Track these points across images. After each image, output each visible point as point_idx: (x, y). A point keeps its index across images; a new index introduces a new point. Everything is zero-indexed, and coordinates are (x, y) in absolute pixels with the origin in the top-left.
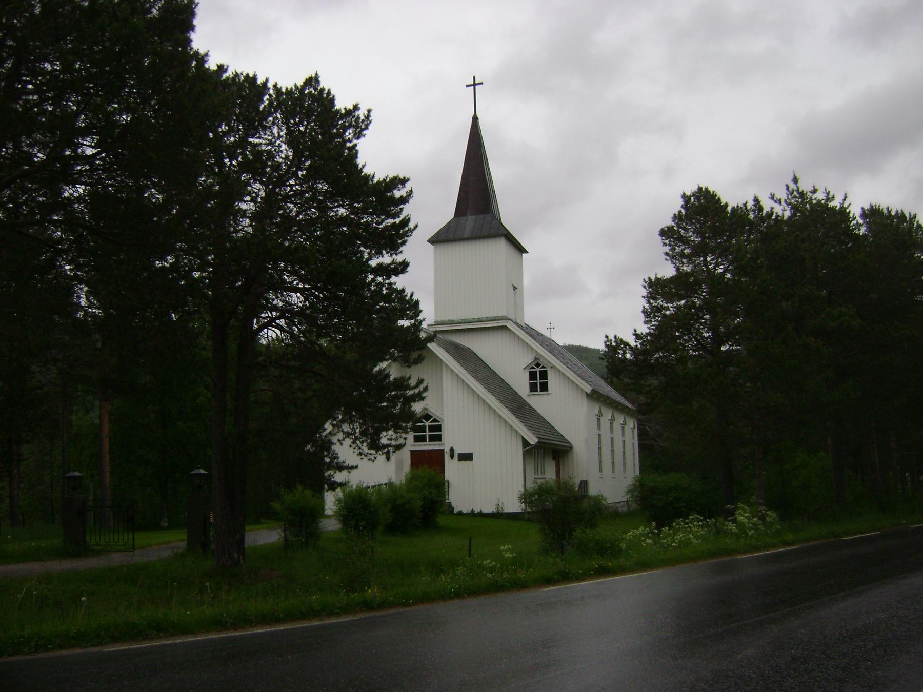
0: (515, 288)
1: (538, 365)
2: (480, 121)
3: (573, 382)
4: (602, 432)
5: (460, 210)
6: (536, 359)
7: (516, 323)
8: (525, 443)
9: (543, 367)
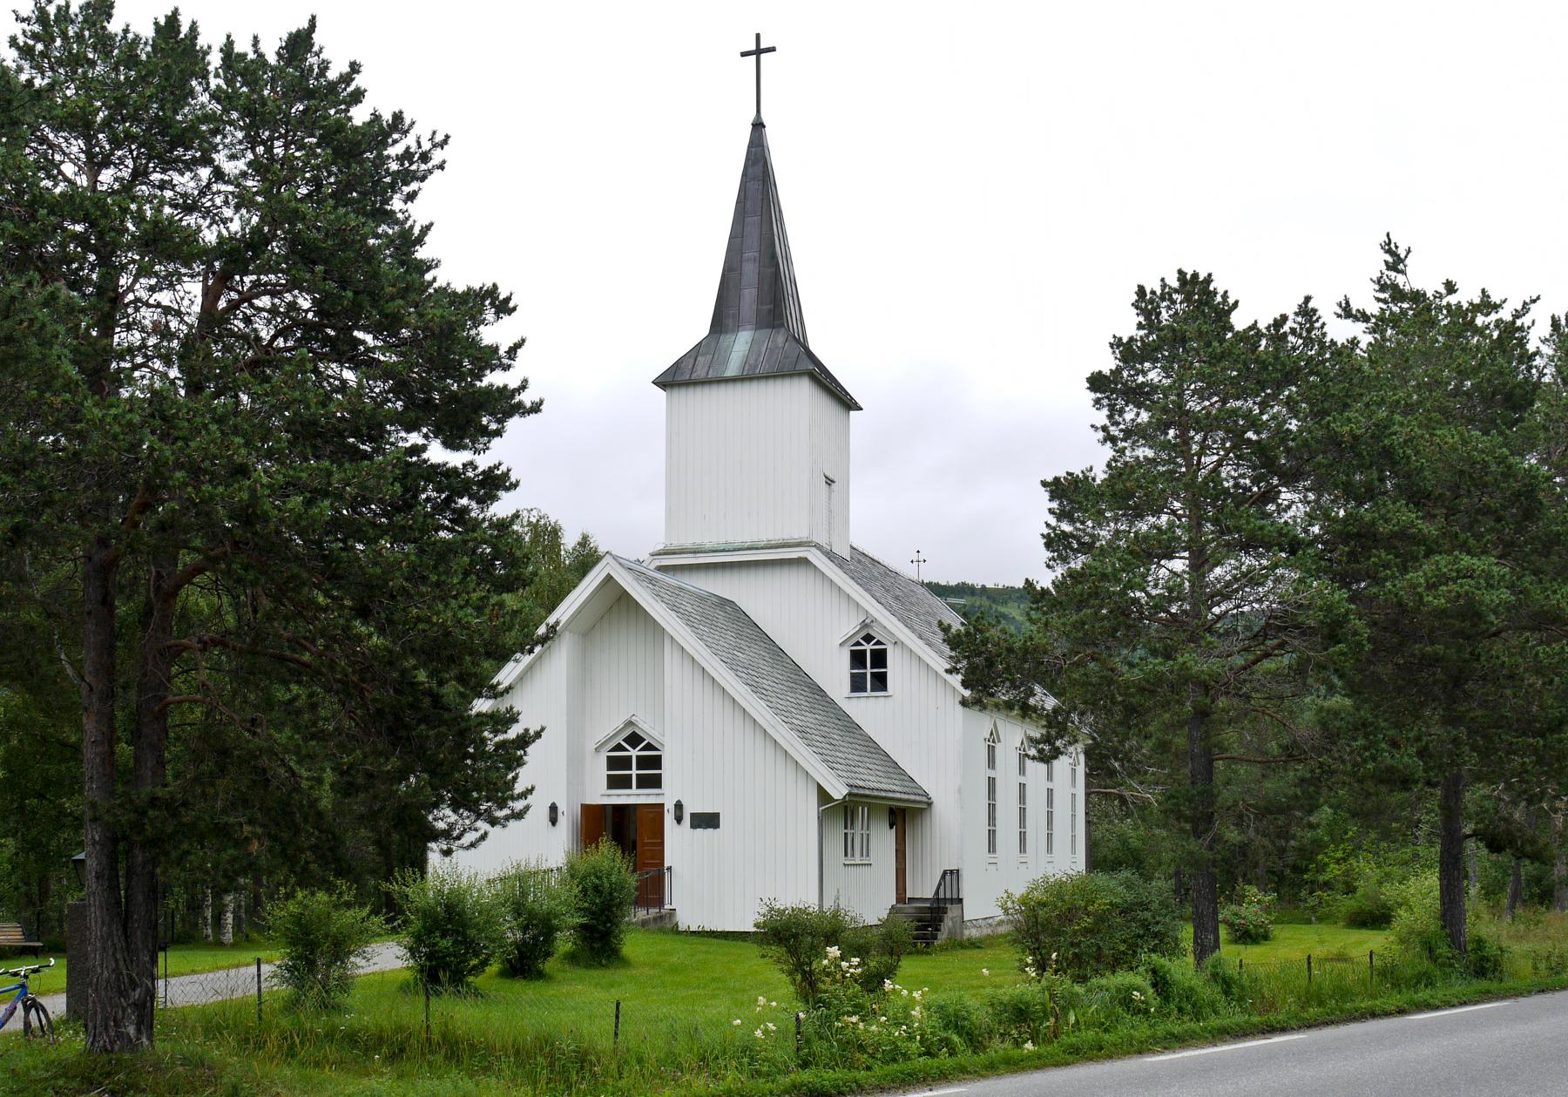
0: (830, 482)
1: (868, 638)
2: (771, 134)
4: (1055, 785)
5: (722, 321)
6: (864, 625)
7: (830, 555)
8: (823, 796)
9: (879, 643)
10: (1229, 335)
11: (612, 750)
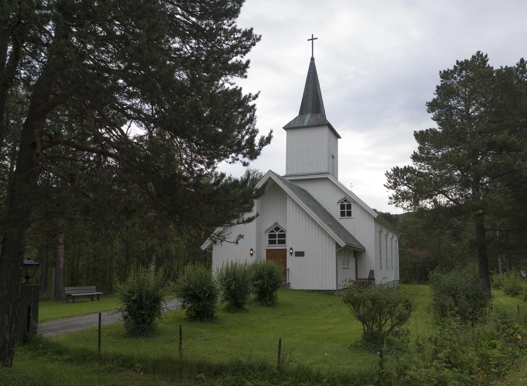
0: (333, 157)
1: (346, 201)
3: (326, 232)
5: (303, 111)
8: (338, 246)
9: (349, 202)
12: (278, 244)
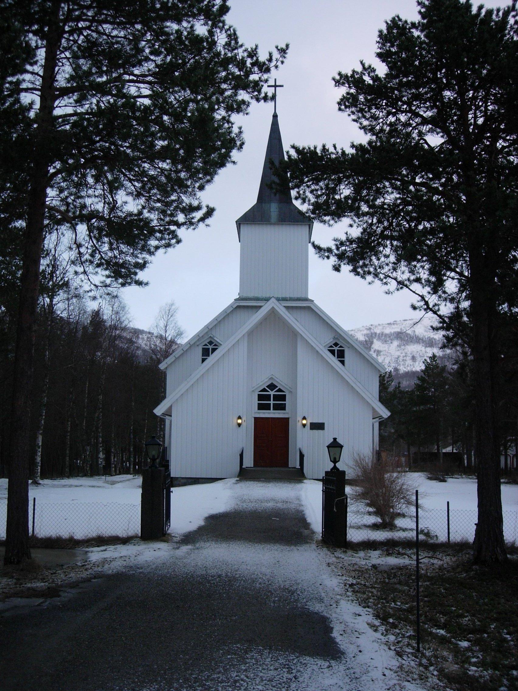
9: (341, 347)
10: (443, 180)
11: (260, 391)
12: (274, 409)
